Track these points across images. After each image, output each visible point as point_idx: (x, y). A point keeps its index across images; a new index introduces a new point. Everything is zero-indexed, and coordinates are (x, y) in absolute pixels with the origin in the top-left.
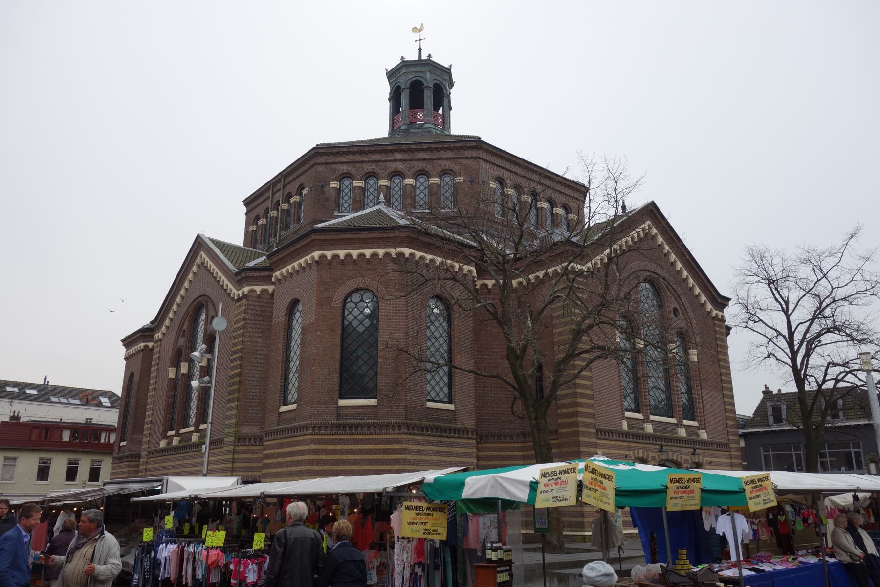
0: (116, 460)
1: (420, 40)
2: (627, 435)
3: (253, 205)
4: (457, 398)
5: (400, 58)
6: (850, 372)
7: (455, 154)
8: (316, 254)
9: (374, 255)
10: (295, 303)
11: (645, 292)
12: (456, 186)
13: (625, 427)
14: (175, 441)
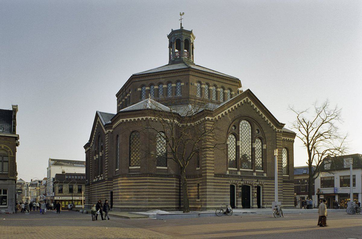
0: (86, 186)
1: (181, 19)
2: (228, 176)
3: (119, 96)
4: (168, 165)
5: (171, 30)
6: (328, 150)
7: (181, 74)
8: (121, 120)
9: (127, 120)
10: (118, 136)
11: (244, 125)
12: (181, 86)
13: (228, 173)
14: (100, 179)
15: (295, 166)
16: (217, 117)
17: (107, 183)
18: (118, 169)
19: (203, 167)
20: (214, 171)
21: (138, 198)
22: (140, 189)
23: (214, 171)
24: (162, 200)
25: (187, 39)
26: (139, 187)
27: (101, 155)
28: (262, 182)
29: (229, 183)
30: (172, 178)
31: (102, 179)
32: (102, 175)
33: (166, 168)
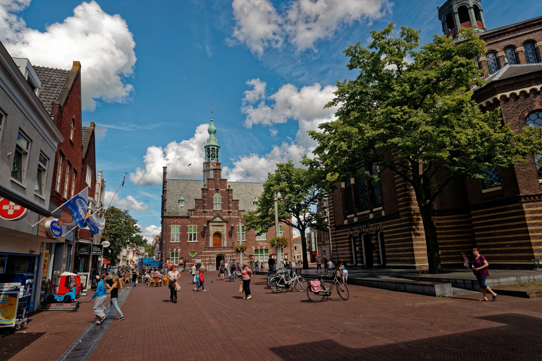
17: (335, 233)
28: (379, 227)
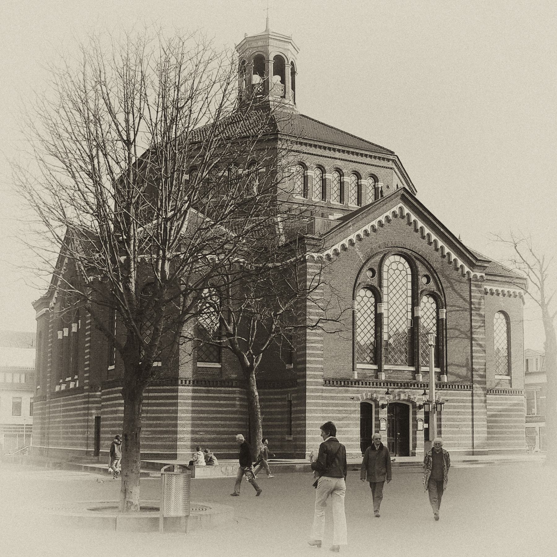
11: (394, 266)
14: (72, 385)
15: (238, 460)
16: (330, 252)
18: (113, 367)
19: (299, 363)
20: (322, 373)
21: (155, 432)
22: (161, 412)
23: (322, 373)
24: (209, 436)
25: (281, 54)
26: (159, 408)
27: (74, 329)
29: (358, 399)
30: (230, 389)
31: (77, 386)
32: (76, 377)
33: (218, 365)
